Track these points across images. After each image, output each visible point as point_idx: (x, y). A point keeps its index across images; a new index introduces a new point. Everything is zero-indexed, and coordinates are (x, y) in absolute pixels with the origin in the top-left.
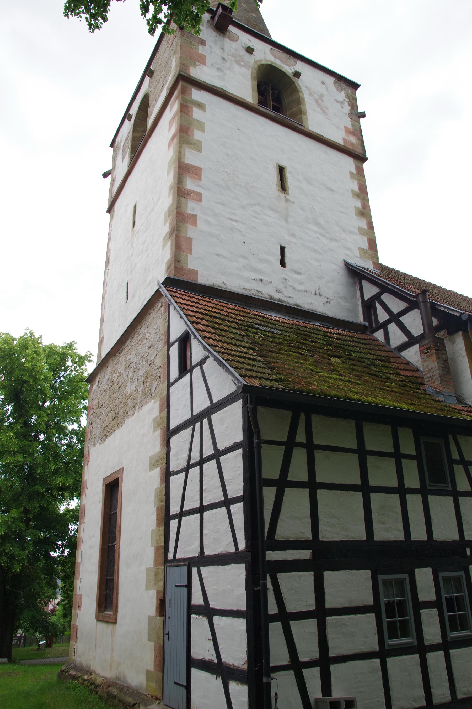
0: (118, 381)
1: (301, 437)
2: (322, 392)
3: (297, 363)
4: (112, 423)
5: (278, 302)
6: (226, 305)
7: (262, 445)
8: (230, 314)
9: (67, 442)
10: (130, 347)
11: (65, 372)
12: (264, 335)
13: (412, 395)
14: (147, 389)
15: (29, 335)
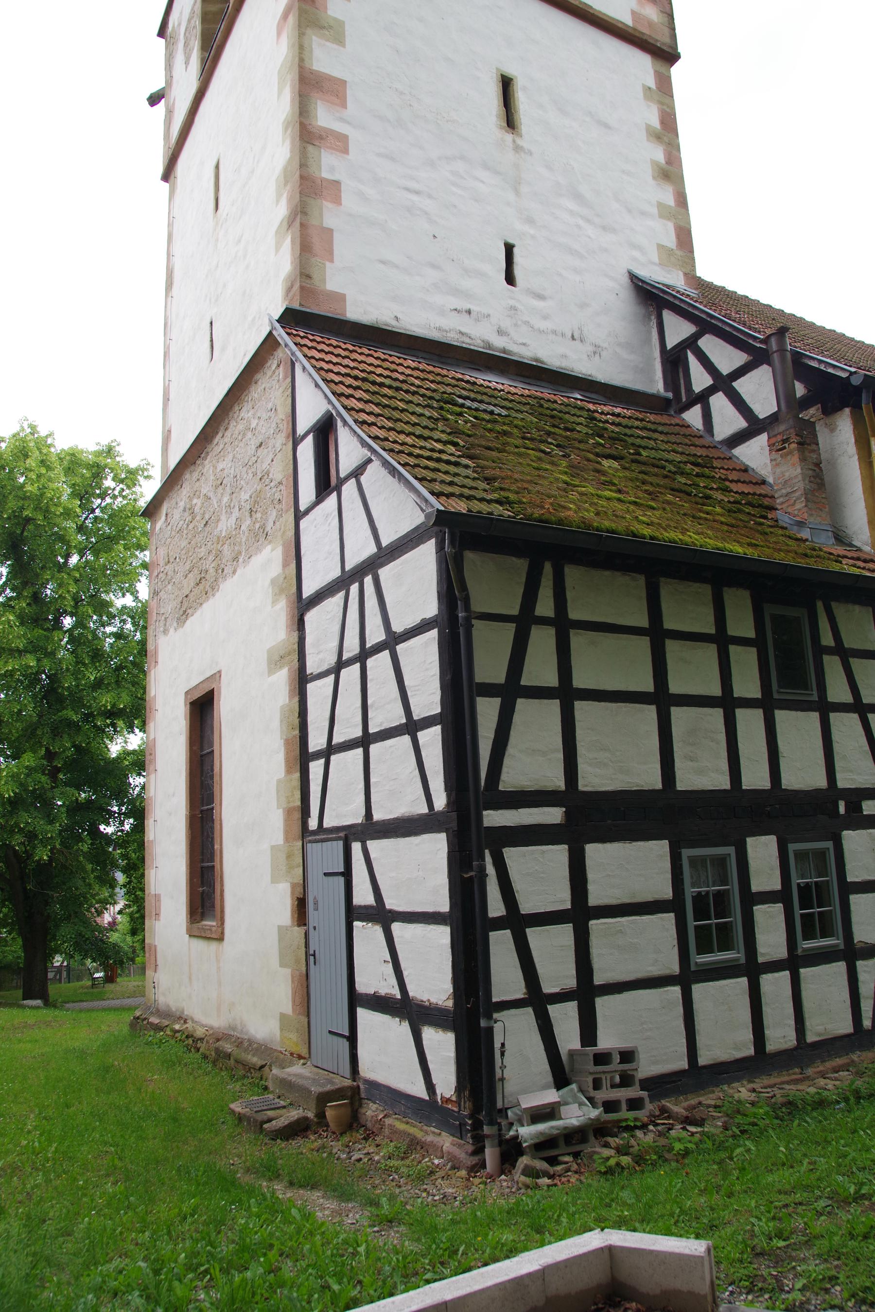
0: (202, 512)
1: (545, 607)
2: (584, 523)
3: (538, 469)
4: (196, 591)
5: (502, 355)
6: (401, 361)
7: (474, 622)
8: (409, 378)
9: (115, 630)
10: (221, 446)
11: (103, 499)
12: (475, 418)
13: (751, 528)
14: (257, 526)
15: (29, 430)
